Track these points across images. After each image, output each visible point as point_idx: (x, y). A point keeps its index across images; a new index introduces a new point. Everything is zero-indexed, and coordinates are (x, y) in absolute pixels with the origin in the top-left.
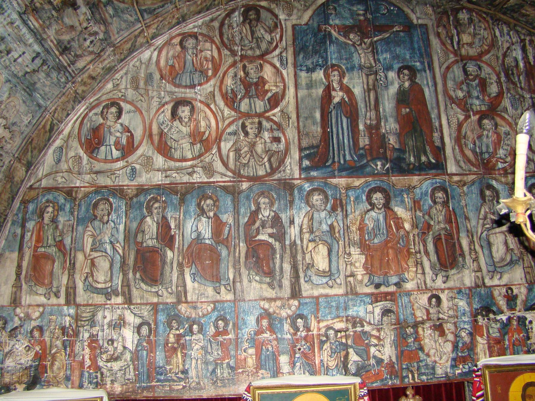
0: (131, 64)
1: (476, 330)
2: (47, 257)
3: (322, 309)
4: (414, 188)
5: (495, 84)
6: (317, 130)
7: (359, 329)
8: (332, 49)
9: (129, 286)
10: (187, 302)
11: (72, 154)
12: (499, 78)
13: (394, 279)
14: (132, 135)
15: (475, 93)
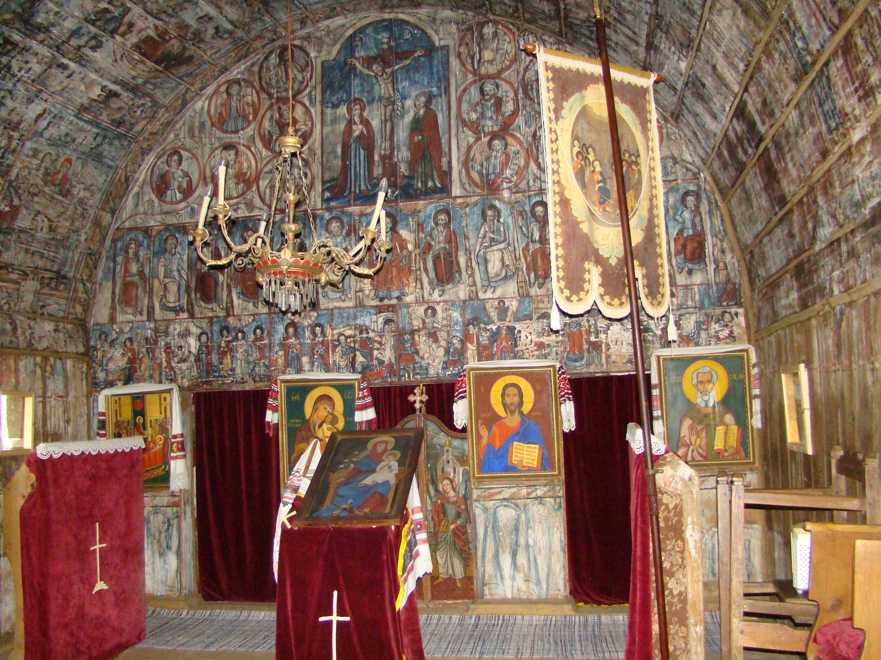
0: (188, 114)
1: (467, 338)
2: (133, 284)
3: (336, 319)
4: (419, 212)
5: (511, 102)
6: (338, 163)
7: (364, 335)
8: (356, 82)
9: (192, 304)
10: (234, 315)
11: (146, 198)
12: (516, 95)
13: (396, 294)
14: (191, 180)
15: (489, 114)
